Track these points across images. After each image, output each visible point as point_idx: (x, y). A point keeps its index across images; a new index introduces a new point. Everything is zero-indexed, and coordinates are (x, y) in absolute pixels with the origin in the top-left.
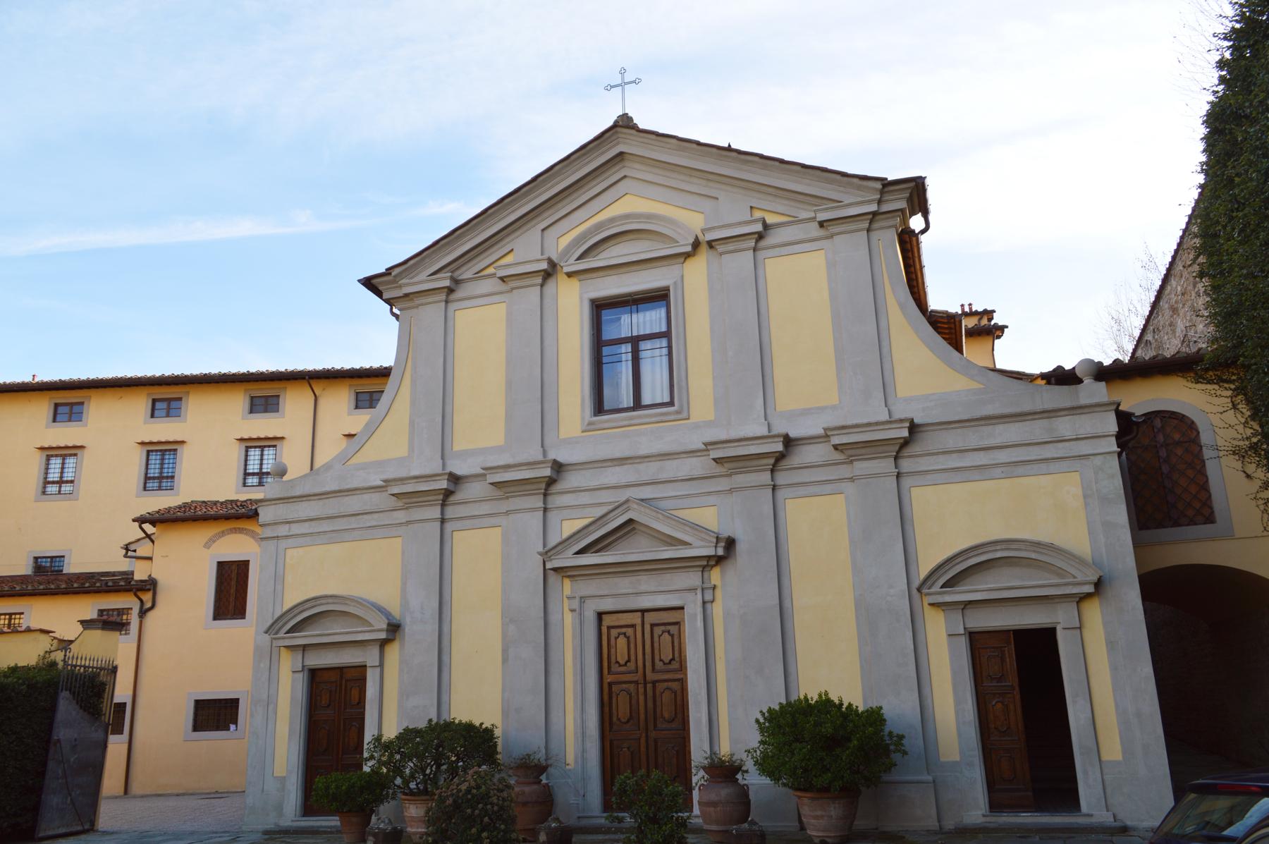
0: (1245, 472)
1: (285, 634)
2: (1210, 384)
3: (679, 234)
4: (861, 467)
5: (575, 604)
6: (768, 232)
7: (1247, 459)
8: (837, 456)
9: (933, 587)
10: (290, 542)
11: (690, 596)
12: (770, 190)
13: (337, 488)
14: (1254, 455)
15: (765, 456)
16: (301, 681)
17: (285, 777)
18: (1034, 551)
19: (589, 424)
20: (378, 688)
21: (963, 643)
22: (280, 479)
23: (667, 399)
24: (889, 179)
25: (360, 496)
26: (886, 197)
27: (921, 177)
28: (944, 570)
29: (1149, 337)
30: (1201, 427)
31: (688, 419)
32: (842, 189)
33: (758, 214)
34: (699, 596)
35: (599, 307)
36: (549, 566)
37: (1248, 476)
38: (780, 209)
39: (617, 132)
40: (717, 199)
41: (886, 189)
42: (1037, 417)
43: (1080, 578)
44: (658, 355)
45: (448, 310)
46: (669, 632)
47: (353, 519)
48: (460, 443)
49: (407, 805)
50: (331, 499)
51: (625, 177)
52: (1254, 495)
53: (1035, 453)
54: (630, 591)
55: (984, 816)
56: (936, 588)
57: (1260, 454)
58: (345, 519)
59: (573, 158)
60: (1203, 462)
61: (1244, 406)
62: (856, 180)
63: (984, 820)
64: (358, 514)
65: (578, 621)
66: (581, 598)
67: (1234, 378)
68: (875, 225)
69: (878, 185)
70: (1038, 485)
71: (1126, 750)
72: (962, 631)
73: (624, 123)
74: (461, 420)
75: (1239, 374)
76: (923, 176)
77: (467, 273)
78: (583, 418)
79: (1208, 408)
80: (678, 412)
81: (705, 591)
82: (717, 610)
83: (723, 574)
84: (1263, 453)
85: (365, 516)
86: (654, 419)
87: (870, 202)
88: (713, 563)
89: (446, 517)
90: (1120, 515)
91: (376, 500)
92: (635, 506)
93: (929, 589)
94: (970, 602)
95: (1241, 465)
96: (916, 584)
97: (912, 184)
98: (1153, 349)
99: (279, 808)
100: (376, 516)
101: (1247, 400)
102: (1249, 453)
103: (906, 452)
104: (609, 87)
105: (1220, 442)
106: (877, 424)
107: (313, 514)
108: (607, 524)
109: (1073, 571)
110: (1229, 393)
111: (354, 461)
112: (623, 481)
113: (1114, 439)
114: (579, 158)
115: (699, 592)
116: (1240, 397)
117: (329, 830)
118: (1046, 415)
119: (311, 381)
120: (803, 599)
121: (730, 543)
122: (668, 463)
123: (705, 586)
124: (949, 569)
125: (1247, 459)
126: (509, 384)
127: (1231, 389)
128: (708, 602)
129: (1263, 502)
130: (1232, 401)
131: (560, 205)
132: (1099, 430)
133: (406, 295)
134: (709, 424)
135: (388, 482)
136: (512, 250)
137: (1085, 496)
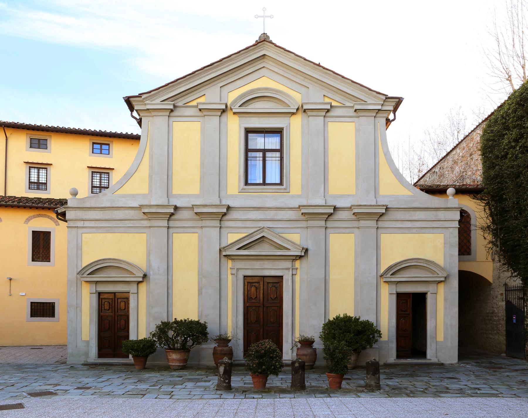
0: (484, 236)
1: (87, 275)
2: (478, 200)
3: (290, 102)
4: (363, 223)
5: (234, 272)
6: (332, 109)
7: (485, 232)
8: (354, 217)
9: (388, 275)
10: (84, 230)
11: (287, 271)
12: (334, 89)
13: (110, 206)
14: (488, 230)
15: (324, 214)
16: (95, 298)
17: (89, 341)
18: (426, 264)
19: (243, 189)
20: (136, 303)
21: (394, 297)
22: (75, 197)
23: (278, 181)
24: (389, 96)
25: (123, 211)
26: (386, 103)
27: (402, 98)
28: (392, 269)
29: (437, 170)
30: (472, 217)
31: (289, 193)
32: (367, 96)
33: (327, 100)
34: (291, 272)
35: (248, 131)
36: (224, 253)
37: (485, 238)
38: (337, 99)
39: (264, 44)
40: (309, 88)
41: (386, 100)
42: (432, 210)
43: (440, 275)
44: (278, 160)
45: (170, 121)
46: (275, 286)
47: (119, 222)
48: (176, 190)
49: (171, 354)
50: (107, 211)
51: (264, 67)
52: (485, 246)
53: (429, 224)
54: (260, 268)
55: (395, 360)
56: (389, 275)
57: (490, 230)
58: (115, 222)
59: (241, 52)
60: (470, 231)
61: (488, 210)
62: (375, 93)
63: (394, 361)
64: (123, 220)
65: (235, 279)
66: (237, 269)
67: (486, 199)
68: (378, 115)
69: (384, 98)
70: (429, 237)
71: (445, 338)
72: (395, 293)
73: (264, 40)
74: (176, 178)
75: (488, 197)
76: (403, 98)
77: (180, 103)
78: (239, 186)
79: (476, 210)
80: (285, 189)
81: (293, 270)
82: (297, 278)
83: (301, 263)
84: (491, 229)
85: (126, 221)
86: (274, 191)
87: (378, 104)
88: (298, 258)
89: (170, 226)
90: (455, 251)
91: (131, 214)
92: (266, 230)
93: (386, 275)
94: (400, 282)
95: (483, 234)
96: (379, 274)
97: (398, 100)
98: (437, 176)
99: (87, 354)
100: (132, 222)
101: (489, 208)
102: (487, 229)
103: (381, 219)
104: (257, 17)
105: (478, 224)
106: (371, 206)
107: (97, 217)
108: (252, 237)
109: (438, 272)
110: (484, 205)
111: (118, 192)
112: (259, 218)
113: (457, 222)
114: (244, 53)
115: (291, 270)
116: (487, 207)
117: (118, 364)
118: (435, 210)
119: (6, 128)
120: (334, 276)
121: (307, 250)
122: (279, 212)
123: (293, 268)
124: (395, 268)
125: (485, 232)
126: (202, 164)
127: (485, 203)
128: (294, 275)
129: (488, 248)
130: (484, 208)
131: (231, 76)
132: (454, 218)
133: (148, 109)
134: (298, 196)
135: (141, 207)
136: (205, 94)
137: (445, 244)
